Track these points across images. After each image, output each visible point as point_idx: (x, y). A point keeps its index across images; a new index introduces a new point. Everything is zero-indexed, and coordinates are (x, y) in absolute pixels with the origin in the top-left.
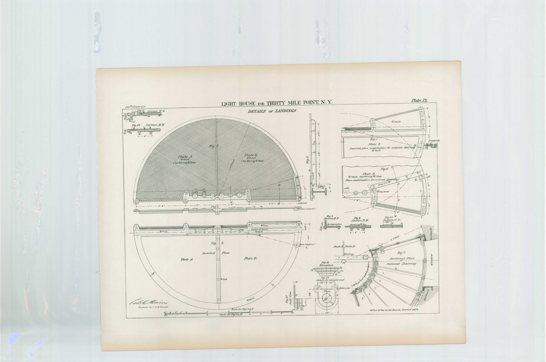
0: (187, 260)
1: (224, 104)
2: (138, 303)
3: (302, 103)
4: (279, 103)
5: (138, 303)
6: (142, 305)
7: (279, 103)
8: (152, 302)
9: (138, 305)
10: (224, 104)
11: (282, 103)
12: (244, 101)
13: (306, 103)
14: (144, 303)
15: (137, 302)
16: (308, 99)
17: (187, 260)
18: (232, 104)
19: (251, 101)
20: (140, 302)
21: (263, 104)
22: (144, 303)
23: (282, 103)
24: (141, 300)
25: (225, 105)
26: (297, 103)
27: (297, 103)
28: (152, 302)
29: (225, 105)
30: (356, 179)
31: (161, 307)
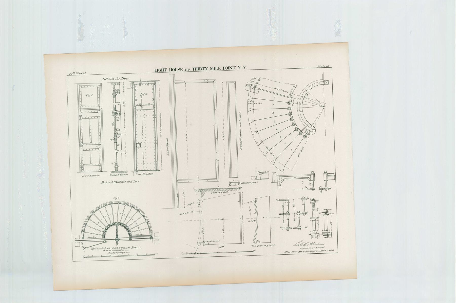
0: (128, 182)
1: (156, 70)
3: (222, 68)
4: (202, 69)
7: (202, 69)
8: (311, 244)
9: (300, 247)
10: (156, 70)
11: (205, 69)
12: (173, 67)
13: (225, 69)
15: (299, 244)
16: (196, 66)
17: (128, 182)
18: (163, 70)
19: (179, 67)
20: (302, 244)
21: (189, 70)
23: (205, 69)
24: (302, 242)
25: (157, 71)
26: (217, 68)
27: (217, 68)
28: (311, 244)
29: (157, 71)
30: (238, 124)
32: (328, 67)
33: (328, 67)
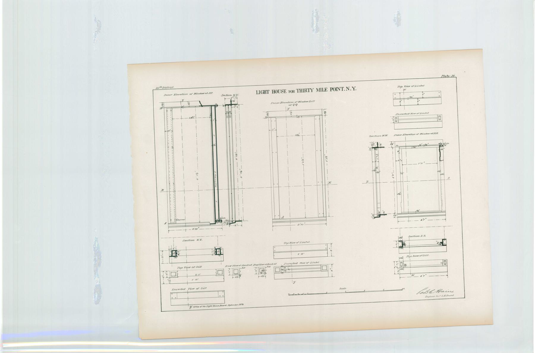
2: (425, 293)
5: (425, 293)
6: (428, 295)
8: (438, 291)
9: (425, 295)
10: (258, 92)
11: (310, 90)
14: (430, 292)
15: (424, 291)
22: (430, 292)
23: (310, 90)
24: (427, 290)
27: (324, 90)
28: (438, 291)
31: (448, 295)
32: (453, 76)
33: (453, 76)
